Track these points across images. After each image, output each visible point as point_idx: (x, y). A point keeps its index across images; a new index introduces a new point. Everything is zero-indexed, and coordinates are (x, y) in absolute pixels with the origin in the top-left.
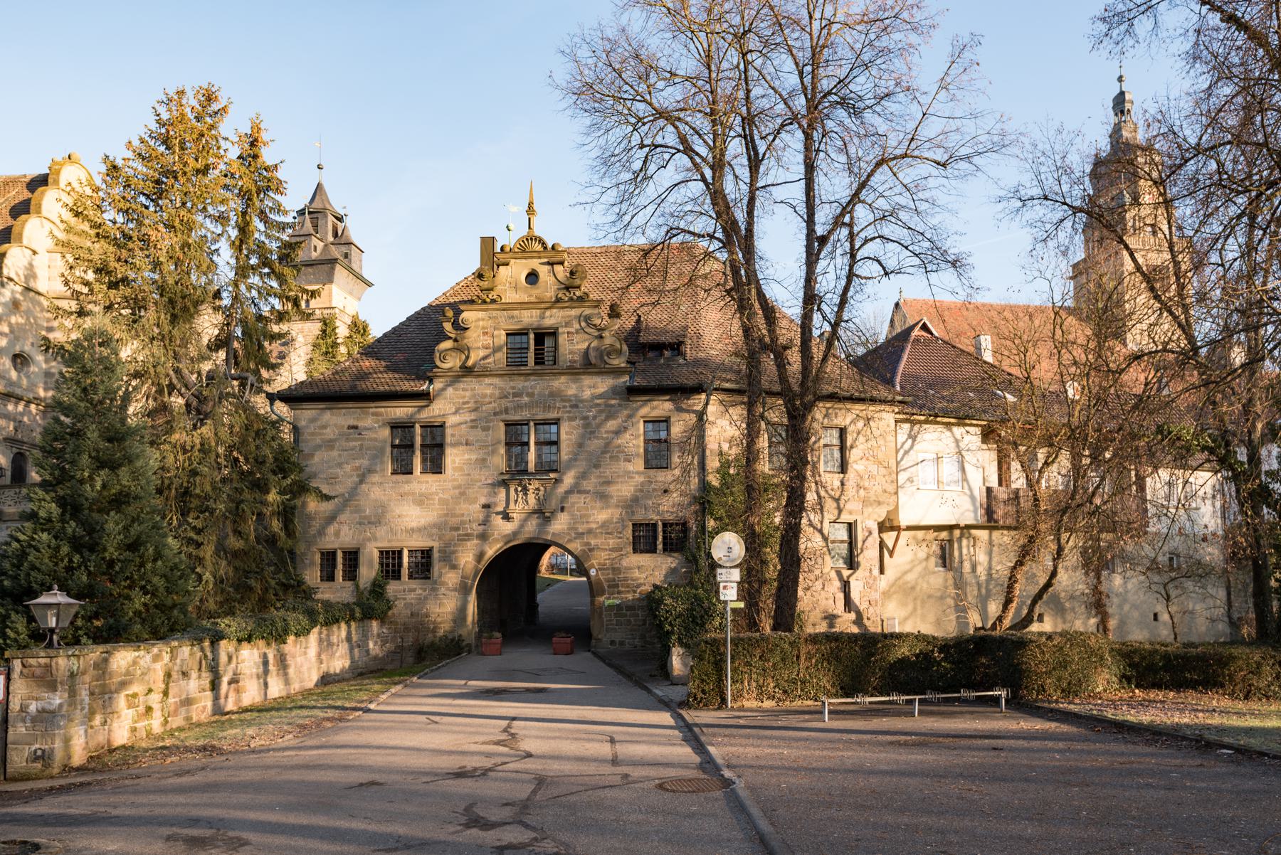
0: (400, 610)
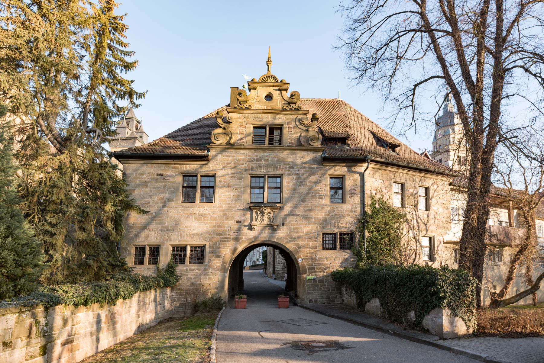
0: (184, 283)
